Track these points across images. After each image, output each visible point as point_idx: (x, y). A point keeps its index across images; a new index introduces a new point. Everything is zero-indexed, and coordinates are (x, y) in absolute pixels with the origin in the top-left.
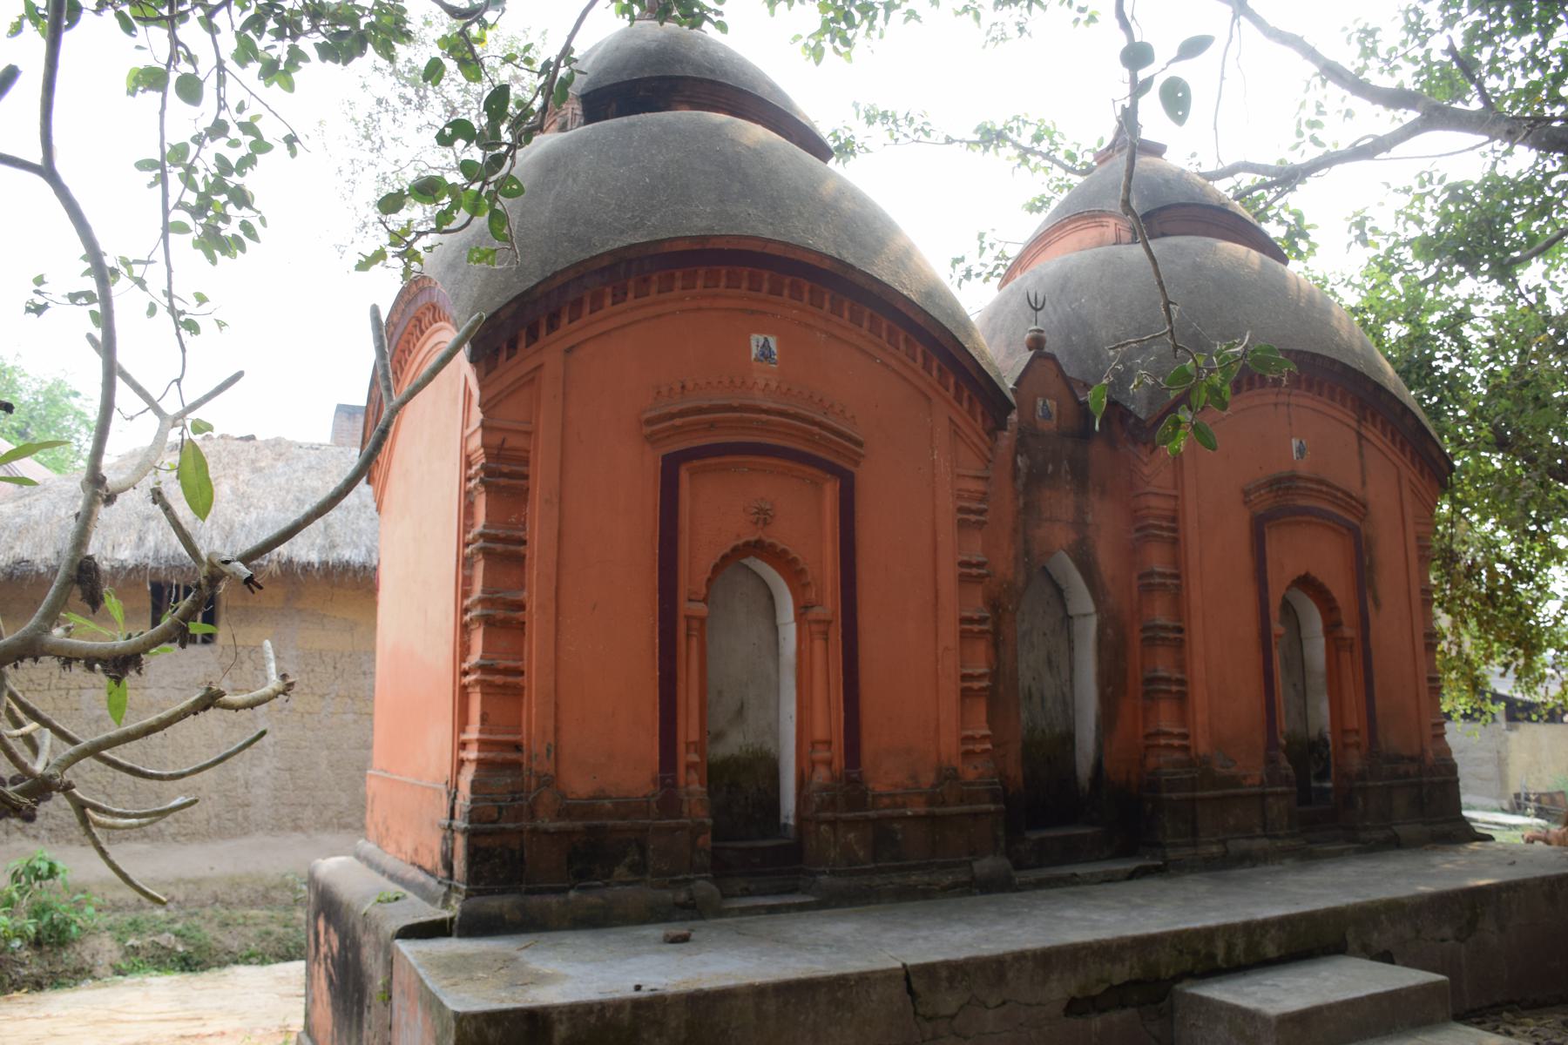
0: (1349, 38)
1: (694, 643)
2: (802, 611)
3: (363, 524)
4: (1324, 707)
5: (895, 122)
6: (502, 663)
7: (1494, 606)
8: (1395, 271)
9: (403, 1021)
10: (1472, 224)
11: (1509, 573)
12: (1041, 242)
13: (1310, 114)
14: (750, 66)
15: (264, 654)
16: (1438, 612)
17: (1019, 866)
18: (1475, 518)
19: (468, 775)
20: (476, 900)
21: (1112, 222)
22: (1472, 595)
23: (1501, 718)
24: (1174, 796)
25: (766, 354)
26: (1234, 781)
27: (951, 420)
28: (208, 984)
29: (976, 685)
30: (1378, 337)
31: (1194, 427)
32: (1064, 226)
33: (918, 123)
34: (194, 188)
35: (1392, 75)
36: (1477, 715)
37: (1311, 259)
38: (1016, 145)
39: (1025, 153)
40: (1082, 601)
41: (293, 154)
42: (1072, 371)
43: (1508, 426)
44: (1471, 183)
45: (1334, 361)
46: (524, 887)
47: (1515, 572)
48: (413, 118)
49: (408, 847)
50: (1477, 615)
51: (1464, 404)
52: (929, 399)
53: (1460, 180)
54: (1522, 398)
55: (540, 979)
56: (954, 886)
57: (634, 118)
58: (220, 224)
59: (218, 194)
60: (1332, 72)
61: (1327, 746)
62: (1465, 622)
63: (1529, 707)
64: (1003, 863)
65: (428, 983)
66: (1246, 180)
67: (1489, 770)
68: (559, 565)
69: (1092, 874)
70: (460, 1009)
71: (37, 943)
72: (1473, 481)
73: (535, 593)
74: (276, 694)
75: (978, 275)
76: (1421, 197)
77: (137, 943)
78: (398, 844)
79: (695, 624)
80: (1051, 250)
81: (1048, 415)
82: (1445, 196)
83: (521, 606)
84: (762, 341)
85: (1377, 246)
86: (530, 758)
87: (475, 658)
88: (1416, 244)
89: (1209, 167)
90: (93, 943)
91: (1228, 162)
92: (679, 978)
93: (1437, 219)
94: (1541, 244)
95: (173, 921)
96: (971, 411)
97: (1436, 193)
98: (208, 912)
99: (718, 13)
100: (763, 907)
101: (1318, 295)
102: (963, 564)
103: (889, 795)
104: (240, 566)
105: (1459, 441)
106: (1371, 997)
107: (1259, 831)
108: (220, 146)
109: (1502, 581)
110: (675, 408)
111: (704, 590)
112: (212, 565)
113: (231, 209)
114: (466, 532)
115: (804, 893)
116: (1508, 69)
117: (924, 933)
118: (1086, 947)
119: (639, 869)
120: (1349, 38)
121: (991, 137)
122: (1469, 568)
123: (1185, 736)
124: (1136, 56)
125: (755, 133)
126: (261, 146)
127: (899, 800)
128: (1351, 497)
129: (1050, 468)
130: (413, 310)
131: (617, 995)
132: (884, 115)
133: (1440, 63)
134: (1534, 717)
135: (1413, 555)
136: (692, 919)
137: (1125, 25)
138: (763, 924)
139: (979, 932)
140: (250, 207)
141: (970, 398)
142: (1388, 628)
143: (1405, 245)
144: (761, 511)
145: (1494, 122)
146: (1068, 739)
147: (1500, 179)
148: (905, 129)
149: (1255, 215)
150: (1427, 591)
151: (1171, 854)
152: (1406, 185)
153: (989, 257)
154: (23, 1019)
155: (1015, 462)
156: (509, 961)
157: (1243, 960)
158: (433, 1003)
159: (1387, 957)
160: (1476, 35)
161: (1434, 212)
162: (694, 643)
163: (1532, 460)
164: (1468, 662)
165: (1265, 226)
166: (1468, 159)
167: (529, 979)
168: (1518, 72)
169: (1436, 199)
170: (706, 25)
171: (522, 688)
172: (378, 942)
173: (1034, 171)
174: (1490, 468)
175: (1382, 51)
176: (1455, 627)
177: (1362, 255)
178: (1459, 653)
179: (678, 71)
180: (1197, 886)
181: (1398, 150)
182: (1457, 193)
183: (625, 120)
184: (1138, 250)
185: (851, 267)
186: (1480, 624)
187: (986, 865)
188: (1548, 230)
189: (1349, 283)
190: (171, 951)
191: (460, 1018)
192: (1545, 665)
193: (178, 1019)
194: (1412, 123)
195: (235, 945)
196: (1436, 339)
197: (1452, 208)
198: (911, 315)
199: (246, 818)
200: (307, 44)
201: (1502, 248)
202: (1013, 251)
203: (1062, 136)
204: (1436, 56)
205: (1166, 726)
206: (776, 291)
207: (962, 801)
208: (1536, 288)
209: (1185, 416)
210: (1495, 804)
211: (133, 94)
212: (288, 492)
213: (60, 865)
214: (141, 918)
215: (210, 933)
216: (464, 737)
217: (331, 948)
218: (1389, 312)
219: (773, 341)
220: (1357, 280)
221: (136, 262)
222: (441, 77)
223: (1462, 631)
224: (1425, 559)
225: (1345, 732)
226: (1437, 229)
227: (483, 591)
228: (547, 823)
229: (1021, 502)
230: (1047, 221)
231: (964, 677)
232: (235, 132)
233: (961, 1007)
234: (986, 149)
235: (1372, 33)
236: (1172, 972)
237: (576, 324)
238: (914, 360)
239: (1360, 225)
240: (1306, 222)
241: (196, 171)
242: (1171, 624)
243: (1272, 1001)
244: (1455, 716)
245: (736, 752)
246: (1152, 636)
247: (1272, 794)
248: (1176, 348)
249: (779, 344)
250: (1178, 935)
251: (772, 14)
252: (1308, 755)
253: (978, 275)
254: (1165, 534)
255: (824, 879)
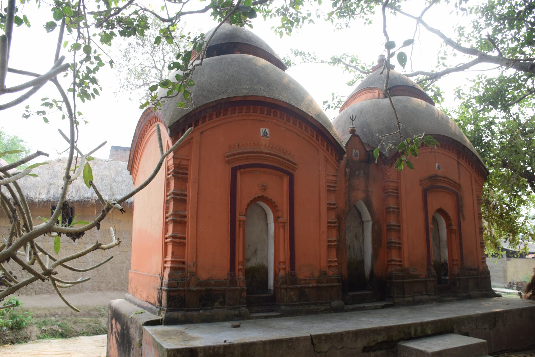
0: (455, 30)
1: (241, 229)
3: (123, 187)
5: (304, 55)
6: (179, 235)
7: (502, 219)
8: (470, 107)
9: (146, 352)
10: (495, 92)
11: (507, 208)
12: (353, 97)
13: (442, 55)
14: (260, 39)
15: (110, 231)
16: (484, 221)
17: (346, 304)
18: (496, 189)
19: (167, 272)
20: (170, 313)
21: (377, 91)
22: (495, 215)
23: (505, 256)
24: (397, 281)
25: (265, 135)
26: (416, 276)
27: (325, 157)
29: (333, 244)
30: (464, 129)
31: (406, 162)
32: (361, 92)
33: (312, 55)
34: (79, 78)
35: (469, 42)
36: (496, 255)
37: (442, 103)
38: (344, 63)
39: (347, 66)
40: (367, 216)
41: (112, 67)
42: (364, 141)
43: (507, 159)
44: (495, 78)
45: (450, 138)
47: (509, 207)
48: (141, 50)
49: (145, 296)
50: (497, 222)
51: (492, 152)
52: (318, 150)
53: (491, 78)
54: (511, 151)
55: (193, 339)
56: (325, 310)
57: (222, 56)
58: (86, 89)
59: (86, 79)
60: (449, 42)
62: (493, 224)
63: (514, 253)
65: (157, 340)
66: (421, 77)
67: (501, 274)
70: (169, 348)
71: (12, 328)
72: (495, 177)
73: (190, 212)
74: (116, 245)
75: (332, 107)
76: (478, 83)
79: (242, 223)
81: (356, 155)
82: (486, 83)
83: (185, 217)
84: (264, 130)
85: (464, 99)
87: (170, 233)
90: (31, 328)
91: (415, 71)
92: (238, 339)
93: (484, 90)
94: (517, 99)
95: (57, 321)
96: (332, 154)
97: (483, 82)
98: (69, 318)
99: (250, 22)
100: (260, 316)
101: (445, 116)
102: (328, 204)
105: (491, 165)
106: (462, 347)
107: (425, 293)
108: (88, 64)
109: (505, 211)
110: (236, 152)
111: (244, 212)
112: (109, 204)
113: (90, 85)
114: (167, 192)
115: (276, 312)
116: (507, 41)
117: (316, 325)
119: (223, 303)
120: (455, 30)
121: (336, 61)
122: (494, 206)
123: (401, 261)
124: (390, 45)
125: (262, 62)
126: (101, 64)
129: (357, 172)
130: (148, 118)
131: (219, 344)
132: (301, 53)
133: (485, 39)
134: (515, 256)
135: (476, 202)
136: (240, 320)
137: (386, 34)
138: (263, 322)
139: (334, 325)
140: (97, 84)
141: (331, 150)
142: (467, 227)
143: (473, 98)
144: (263, 186)
145: (502, 60)
146: (362, 262)
147: (504, 77)
148: (308, 58)
149: (424, 89)
150: (480, 214)
151: (396, 300)
152: (474, 79)
153: (336, 101)
154: (9, 353)
155: (345, 170)
156: (182, 333)
157: (420, 335)
158: (158, 346)
159: (467, 334)
160: (497, 30)
161: (483, 88)
162: (241, 229)
163: (515, 171)
164: (494, 237)
165: (427, 92)
166: (493, 71)
167: (189, 338)
168: (510, 42)
169: (483, 84)
170: (245, 25)
171: (185, 243)
172: (137, 327)
173: (350, 72)
176: (489, 226)
177: (459, 102)
178: (491, 234)
179: (236, 41)
180: (404, 311)
181: (471, 68)
182: (490, 82)
183: (219, 57)
184: (387, 100)
185: (293, 106)
186: (498, 225)
187: (335, 303)
190: (57, 332)
191: (168, 351)
192: (519, 239)
193: (62, 354)
195: (79, 330)
196: (483, 130)
197: (488, 87)
198: (312, 122)
200: (116, 31)
201: (505, 100)
202: (344, 100)
203: (360, 61)
205: (394, 258)
207: (328, 282)
208: (516, 113)
209: (404, 158)
210: (503, 285)
211: (70, 51)
213: (20, 302)
214: (47, 320)
215: (70, 325)
216: (166, 259)
217: (117, 329)
218: (467, 121)
220: (457, 110)
221: (59, 101)
222: (160, 43)
223: (492, 227)
224: (479, 204)
225: (453, 260)
226: (484, 94)
228: (193, 288)
229: (347, 184)
231: (329, 241)
232: (93, 59)
234: (334, 64)
235: (462, 28)
236: (397, 339)
238: (313, 137)
239: (458, 92)
240: (441, 91)
241: (80, 72)
242: (396, 224)
243: (430, 348)
244: (489, 255)
245: (254, 265)
246: (390, 228)
247: (429, 281)
248: (401, 137)
249: (270, 131)
250: (399, 326)
251: (265, 20)
253: (332, 107)
254: (395, 195)
255: (283, 307)
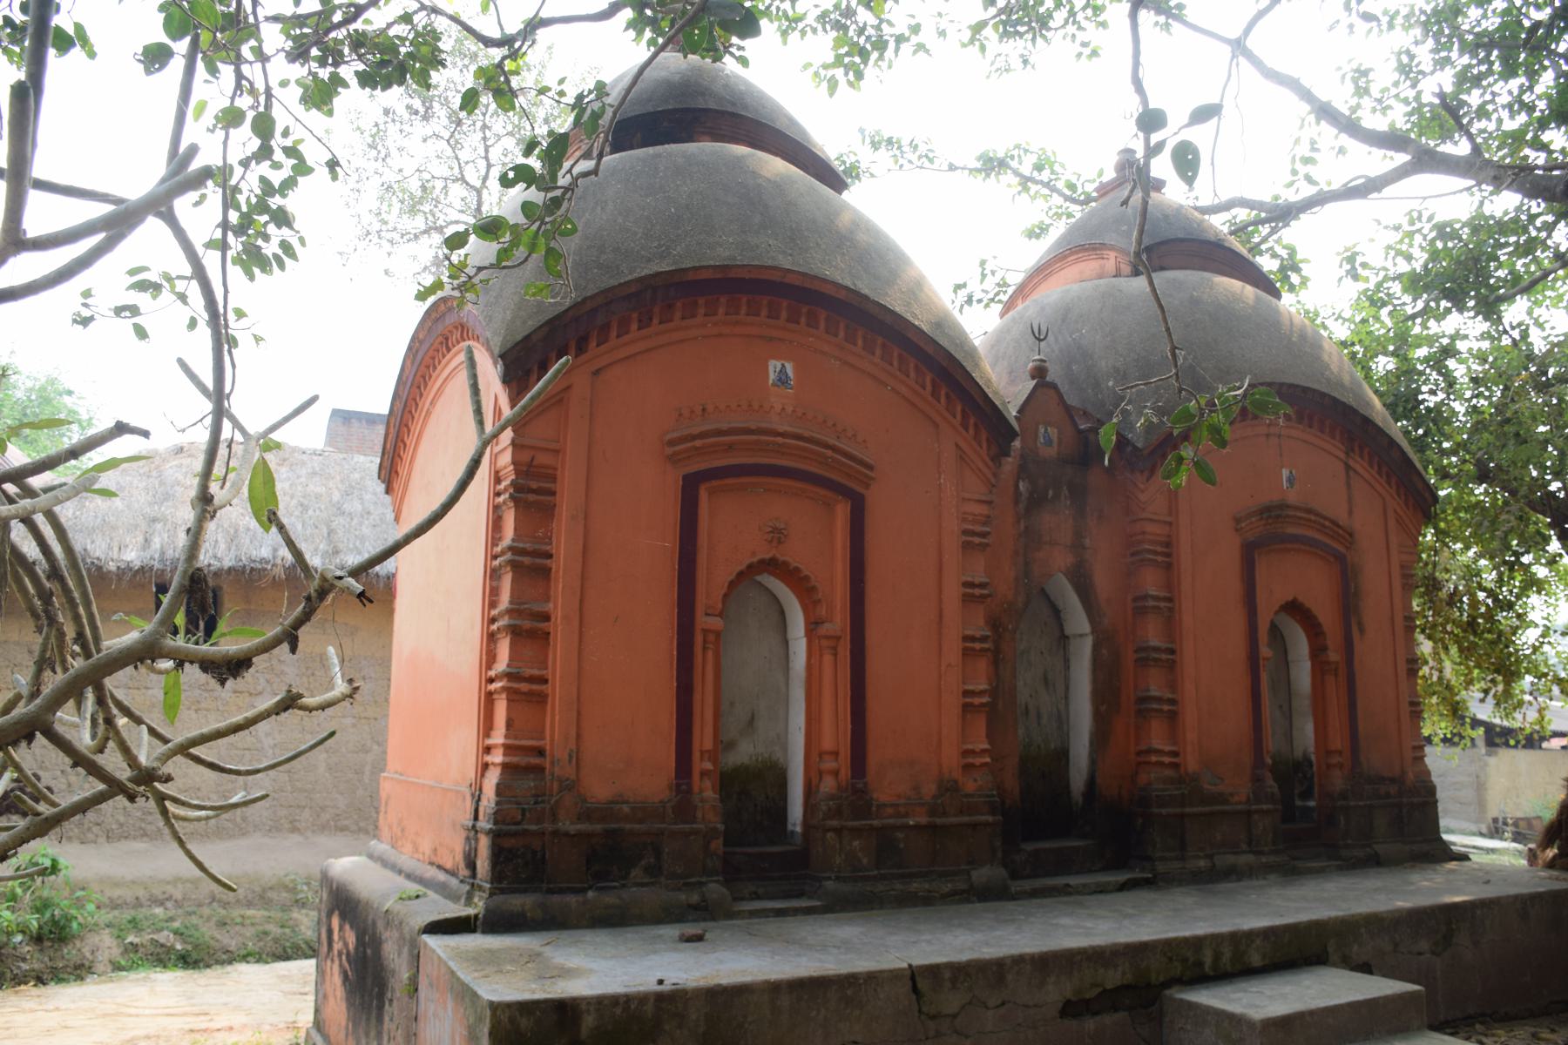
0: (1343, 77)
1: (710, 654)
2: (812, 626)
3: (366, 530)
4: (1309, 728)
5: (899, 148)
6: (528, 672)
7: (1475, 633)
8: (1384, 304)
10: (1458, 262)
11: (1489, 601)
12: (1041, 273)
13: (1304, 150)
14: (769, 99)
15: (327, 658)
16: (1420, 638)
17: (1015, 876)
18: (1459, 546)
19: (492, 779)
20: (499, 899)
21: (1112, 255)
23: (1481, 743)
24: (1164, 811)
25: (783, 379)
26: (1221, 798)
28: (213, 981)
29: (977, 701)
30: (1367, 370)
31: (1196, 464)
32: (1066, 257)
33: (922, 149)
34: (238, 208)
35: (1384, 114)
38: (1016, 173)
39: (1025, 181)
40: (1078, 622)
41: (335, 177)
42: (1072, 400)
44: (1458, 221)
46: (545, 886)
47: (1496, 600)
48: (420, 129)
49: (426, 846)
50: (1458, 641)
52: (936, 425)
55: (565, 973)
56: (954, 893)
57: (659, 149)
58: (260, 242)
59: (260, 214)
60: (1325, 112)
61: (1310, 764)
62: (1446, 649)
63: (1508, 732)
64: (1001, 872)
66: (1243, 214)
68: (583, 578)
69: (1084, 885)
70: (495, 998)
71: (38, 939)
72: (1456, 510)
73: (560, 605)
74: (345, 697)
75: (980, 301)
76: (1411, 234)
77: (137, 940)
78: (415, 844)
79: (711, 637)
80: (1053, 280)
81: (1049, 442)
82: (1434, 234)
85: (1367, 280)
86: (552, 763)
87: (501, 665)
88: (1405, 279)
89: (1205, 202)
90: (93, 939)
91: (1225, 197)
93: (1426, 256)
94: (1524, 284)
95: (172, 919)
97: (1425, 231)
98: (206, 911)
99: (740, 48)
101: (1309, 330)
102: (966, 584)
103: (892, 805)
104: (351, 581)
105: (1444, 475)
107: (1244, 847)
108: (264, 168)
109: (1483, 609)
110: (696, 430)
112: (324, 579)
113: (271, 229)
114: (494, 544)
115: (810, 898)
116: (1495, 110)
117: (927, 937)
118: (1082, 952)
119: (654, 871)
120: (1343, 77)
121: (992, 165)
122: (1452, 596)
123: (1175, 754)
124: (1150, 121)
125: (775, 166)
126: (302, 168)
127: (902, 810)
128: (1338, 526)
129: (1051, 493)
130: (440, 328)
131: (642, 989)
132: (890, 142)
133: (1430, 104)
134: (1512, 742)
135: (1397, 583)
136: (705, 920)
138: (772, 926)
139: (979, 936)
141: (976, 425)
142: (1372, 653)
143: (1394, 279)
144: (775, 530)
145: (1480, 168)
146: (1063, 755)
147: (1487, 219)
149: (1250, 250)
150: (1410, 618)
151: (1161, 867)
152: (1396, 222)
153: (990, 284)
154: (32, 1011)
155: (1017, 487)
156: (534, 957)
157: (1229, 969)
158: (465, 994)
159: (1366, 968)
160: (1467, 80)
161: (1422, 248)
162: (710, 654)
163: (1513, 493)
164: (1449, 687)
165: (1259, 260)
166: (1454, 201)
167: (555, 973)
168: (1505, 114)
169: (1425, 237)
170: (727, 59)
171: (546, 696)
172: (402, 937)
173: (1033, 198)
174: (1473, 499)
175: (1375, 91)
176: (1436, 653)
177: (1353, 289)
178: (1440, 678)
179: (700, 103)
180: (1184, 899)
181: (1388, 191)
183: (651, 150)
184: (1141, 282)
185: (866, 297)
186: (1461, 650)
187: (983, 874)
188: (1533, 268)
189: (1340, 317)
190: (170, 949)
191: (495, 1007)
192: (1523, 692)
193: (185, 1014)
194: (1405, 164)
195: (233, 945)
196: (1421, 373)
197: (1439, 245)
198: (922, 344)
199: (244, 819)
200: (347, 72)
201: (1488, 286)
202: (1015, 279)
203: (1063, 166)
204: (1427, 98)
205: (1157, 744)
206: (794, 319)
208: (1519, 325)
209: (1187, 452)
210: (1474, 828)
211: (212, 131)
212: (292, 497)
213: (62, 862)
214: (140, 916)
215: (208, 933)
216: (489, 742)
217: (346, 944)
219: (789, 368)
220: (1347, 315)
221: (179, 277)
222: (475, 107)
223: (1443, 656)
224: (1408, 588)
225: (1329, 753)
226: (1425, 266)
227: (511, 602)
228: (569, 826)
230: (1049, 251)
231: (966, 693)
232: (278, 155)
233: (963, 1007)
234: (988, 175)
235: (1365, 73)
236: (1162, 979)
237: (603, 348)
239: (1351, 260)
240: (1299, 257)
241: (241, 192)
242: (1164, 645)
244: (1436, 740)
245: (746, 760)
246: (1145, 657)
247: (1257, 811)
249: (796, 369)
250: (1168, 943)
251: (785, 43)
252: (1294, 774)
253: (980, 301)
254: (1160, 559)
255: (829, 885)
